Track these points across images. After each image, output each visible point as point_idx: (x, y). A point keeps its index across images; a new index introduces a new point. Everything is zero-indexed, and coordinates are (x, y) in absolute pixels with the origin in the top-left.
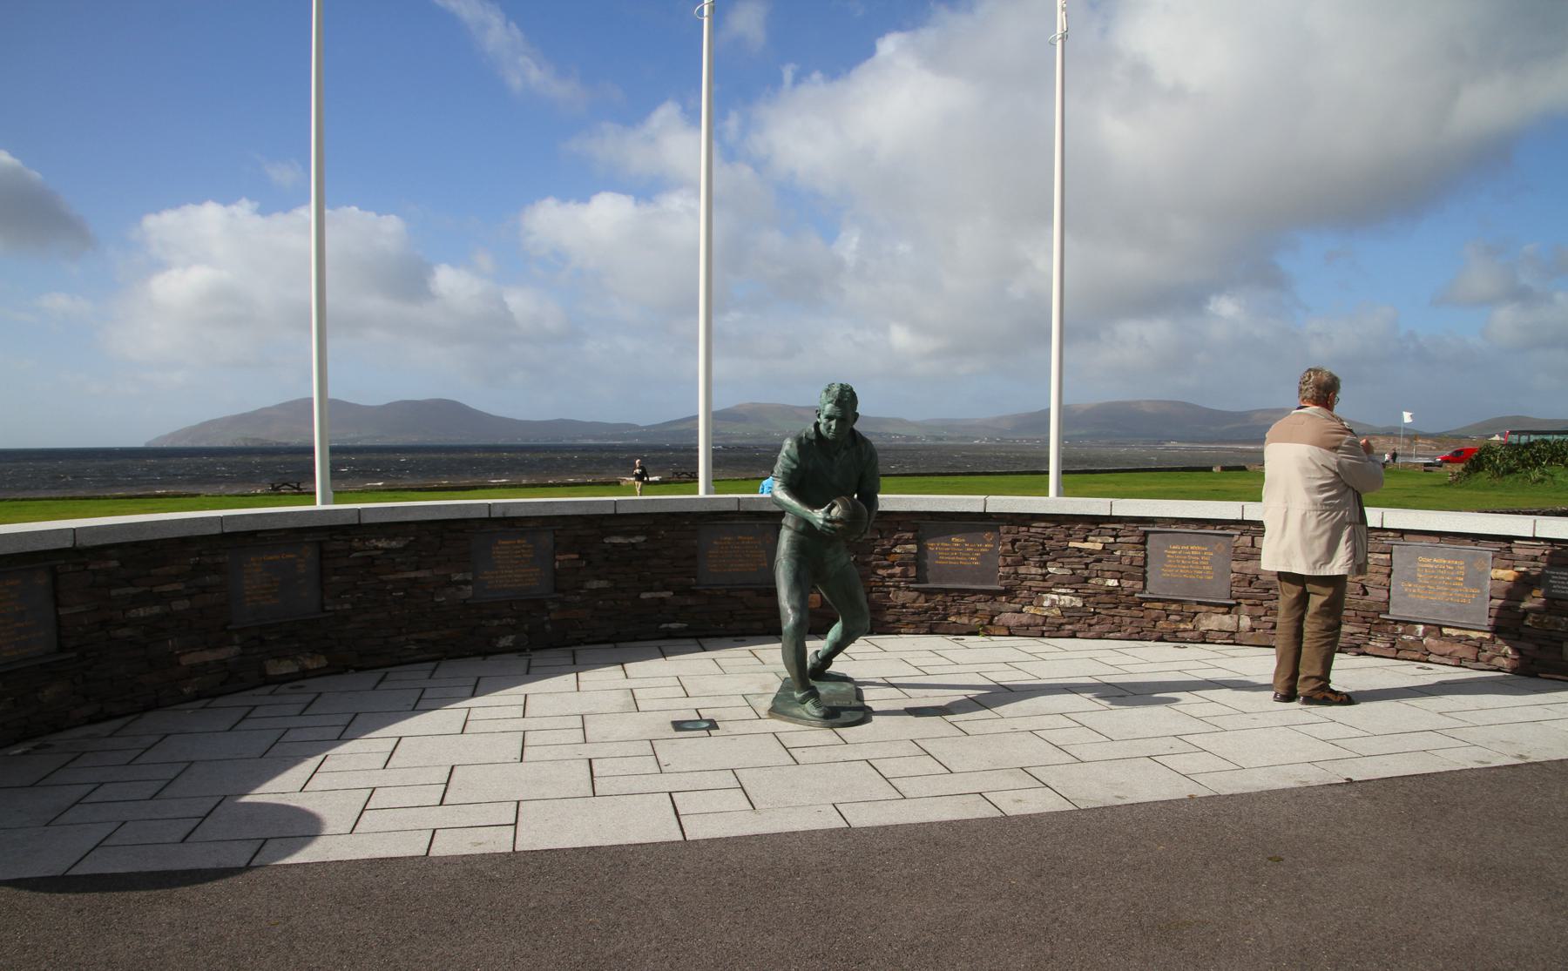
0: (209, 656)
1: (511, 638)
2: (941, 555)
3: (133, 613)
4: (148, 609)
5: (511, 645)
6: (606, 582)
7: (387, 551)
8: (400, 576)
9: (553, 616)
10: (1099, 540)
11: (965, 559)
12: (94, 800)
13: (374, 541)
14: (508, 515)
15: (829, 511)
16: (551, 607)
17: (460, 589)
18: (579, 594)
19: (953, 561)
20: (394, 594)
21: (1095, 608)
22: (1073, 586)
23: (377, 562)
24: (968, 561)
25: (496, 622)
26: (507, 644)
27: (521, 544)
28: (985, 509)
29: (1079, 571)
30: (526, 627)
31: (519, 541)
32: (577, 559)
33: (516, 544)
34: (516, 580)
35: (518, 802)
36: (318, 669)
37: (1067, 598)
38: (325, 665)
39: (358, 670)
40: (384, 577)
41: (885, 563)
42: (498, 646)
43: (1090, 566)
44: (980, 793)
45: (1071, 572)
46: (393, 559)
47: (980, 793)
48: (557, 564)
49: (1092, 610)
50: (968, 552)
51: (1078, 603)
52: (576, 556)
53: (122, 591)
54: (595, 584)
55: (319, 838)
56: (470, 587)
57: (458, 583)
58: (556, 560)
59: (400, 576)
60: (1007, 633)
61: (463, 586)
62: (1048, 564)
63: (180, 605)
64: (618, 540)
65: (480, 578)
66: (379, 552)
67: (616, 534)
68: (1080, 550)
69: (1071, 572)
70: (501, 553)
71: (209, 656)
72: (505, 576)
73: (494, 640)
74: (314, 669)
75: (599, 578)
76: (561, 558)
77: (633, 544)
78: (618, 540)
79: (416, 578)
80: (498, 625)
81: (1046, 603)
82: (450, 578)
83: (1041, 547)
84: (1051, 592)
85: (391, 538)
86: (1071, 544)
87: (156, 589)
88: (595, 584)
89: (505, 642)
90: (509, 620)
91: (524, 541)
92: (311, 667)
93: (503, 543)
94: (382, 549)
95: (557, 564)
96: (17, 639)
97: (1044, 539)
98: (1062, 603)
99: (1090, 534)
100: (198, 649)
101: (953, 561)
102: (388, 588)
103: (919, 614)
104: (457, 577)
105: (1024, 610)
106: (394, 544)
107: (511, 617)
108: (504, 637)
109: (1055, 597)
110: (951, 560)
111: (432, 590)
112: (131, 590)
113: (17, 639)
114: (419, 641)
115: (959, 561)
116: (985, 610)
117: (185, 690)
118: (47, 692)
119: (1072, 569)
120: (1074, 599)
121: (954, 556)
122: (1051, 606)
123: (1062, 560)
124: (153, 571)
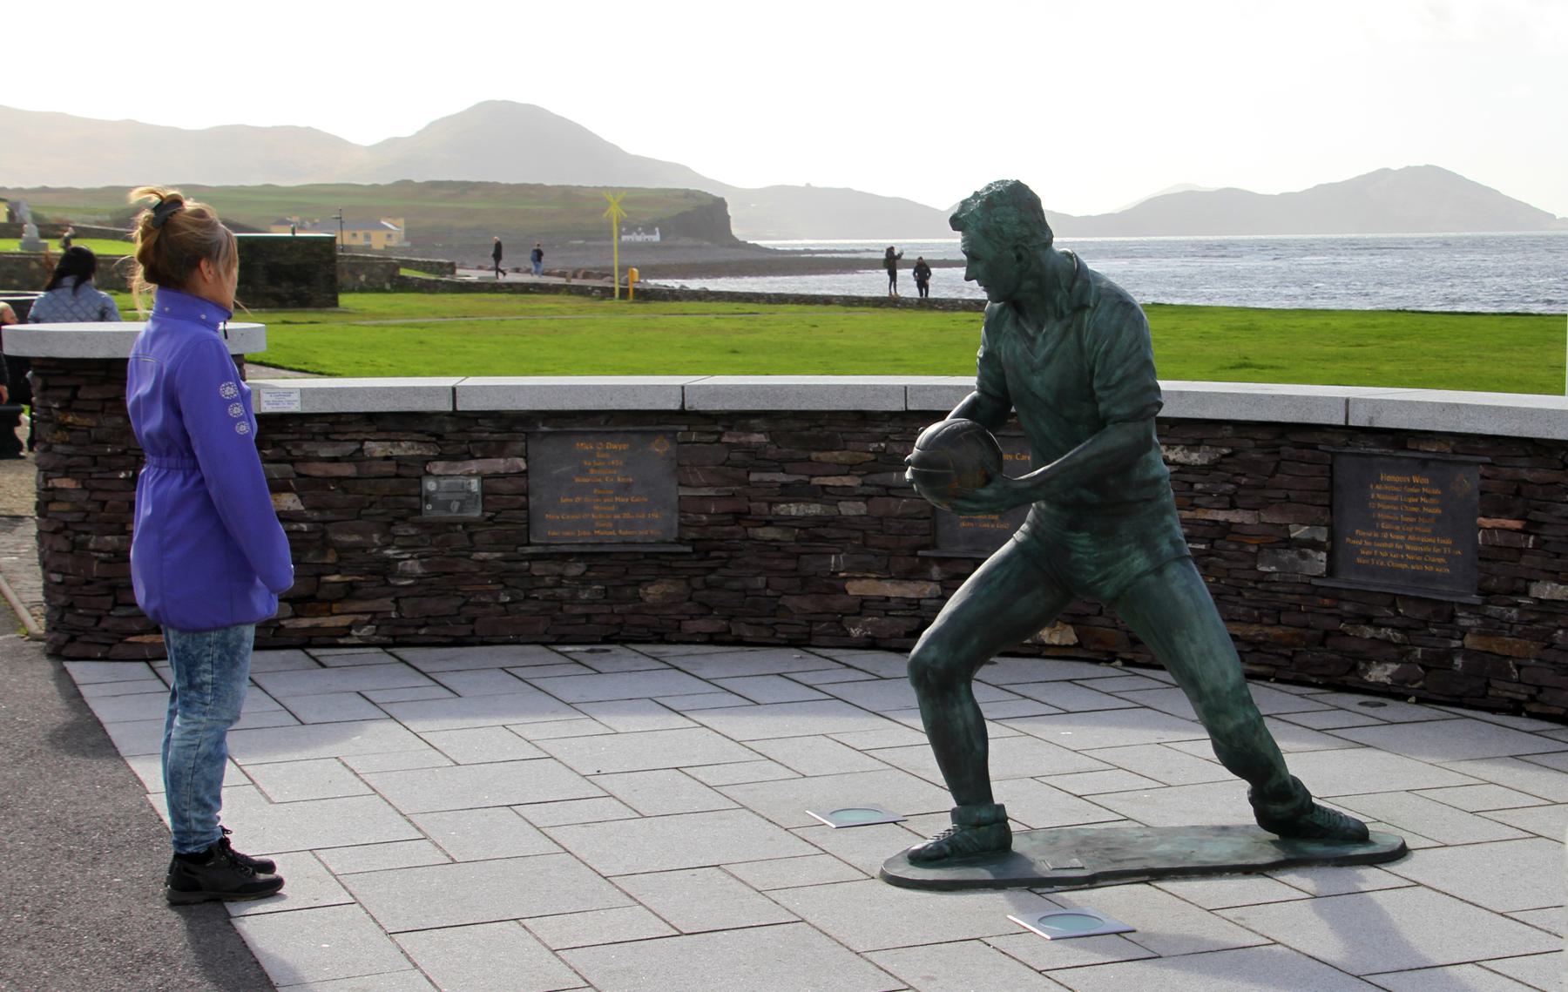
0: (891, 589)
1: (1392, 667)
3: (781, 509)
4: (802, 506)
5: (1389, 681)
9: (1469, 641)
12: (1296, 892)
14: (1376, 425)
16: (1466, 623)
17: (1304, 556)
18: (1518, 605)
25: (1369, 632)
26: (1383, 679)
27: (1419, 486)
30: (1419, 652)
31: (1416, 480)
32: (1518, 531)
33: (1411, 485)
36: (1059, 646)
38: (1071, 643)
39: (1128, 663)
42: (1366, 677)
53: (767, 477)
55: (393, 726)
63: (850, 509)
65: (1348, 539)
70: (1384, 497)
71: (891, 589)
72: (1391, 546)
74: (1053, 646)
76: (1488, 523)
80: (1373, 638)
82: (1288, 531)
85: (1193, 446)
87: (815, 481)
89: (1380, 673)
90: (1389, 631)
91: (1426, 481)
92: (1047, 641)
93: (1389, 478)
96: (618, 517)
100: (874, 576)
104: (1298, 532)
106: (1195, 458)
107: (1394, 628)
108: (1379, 663)
111: (1253, 549)
112: (781, 478)
113: (618, 517)
117: (852, 631)
118: (651, 590)
124: (814, 455)
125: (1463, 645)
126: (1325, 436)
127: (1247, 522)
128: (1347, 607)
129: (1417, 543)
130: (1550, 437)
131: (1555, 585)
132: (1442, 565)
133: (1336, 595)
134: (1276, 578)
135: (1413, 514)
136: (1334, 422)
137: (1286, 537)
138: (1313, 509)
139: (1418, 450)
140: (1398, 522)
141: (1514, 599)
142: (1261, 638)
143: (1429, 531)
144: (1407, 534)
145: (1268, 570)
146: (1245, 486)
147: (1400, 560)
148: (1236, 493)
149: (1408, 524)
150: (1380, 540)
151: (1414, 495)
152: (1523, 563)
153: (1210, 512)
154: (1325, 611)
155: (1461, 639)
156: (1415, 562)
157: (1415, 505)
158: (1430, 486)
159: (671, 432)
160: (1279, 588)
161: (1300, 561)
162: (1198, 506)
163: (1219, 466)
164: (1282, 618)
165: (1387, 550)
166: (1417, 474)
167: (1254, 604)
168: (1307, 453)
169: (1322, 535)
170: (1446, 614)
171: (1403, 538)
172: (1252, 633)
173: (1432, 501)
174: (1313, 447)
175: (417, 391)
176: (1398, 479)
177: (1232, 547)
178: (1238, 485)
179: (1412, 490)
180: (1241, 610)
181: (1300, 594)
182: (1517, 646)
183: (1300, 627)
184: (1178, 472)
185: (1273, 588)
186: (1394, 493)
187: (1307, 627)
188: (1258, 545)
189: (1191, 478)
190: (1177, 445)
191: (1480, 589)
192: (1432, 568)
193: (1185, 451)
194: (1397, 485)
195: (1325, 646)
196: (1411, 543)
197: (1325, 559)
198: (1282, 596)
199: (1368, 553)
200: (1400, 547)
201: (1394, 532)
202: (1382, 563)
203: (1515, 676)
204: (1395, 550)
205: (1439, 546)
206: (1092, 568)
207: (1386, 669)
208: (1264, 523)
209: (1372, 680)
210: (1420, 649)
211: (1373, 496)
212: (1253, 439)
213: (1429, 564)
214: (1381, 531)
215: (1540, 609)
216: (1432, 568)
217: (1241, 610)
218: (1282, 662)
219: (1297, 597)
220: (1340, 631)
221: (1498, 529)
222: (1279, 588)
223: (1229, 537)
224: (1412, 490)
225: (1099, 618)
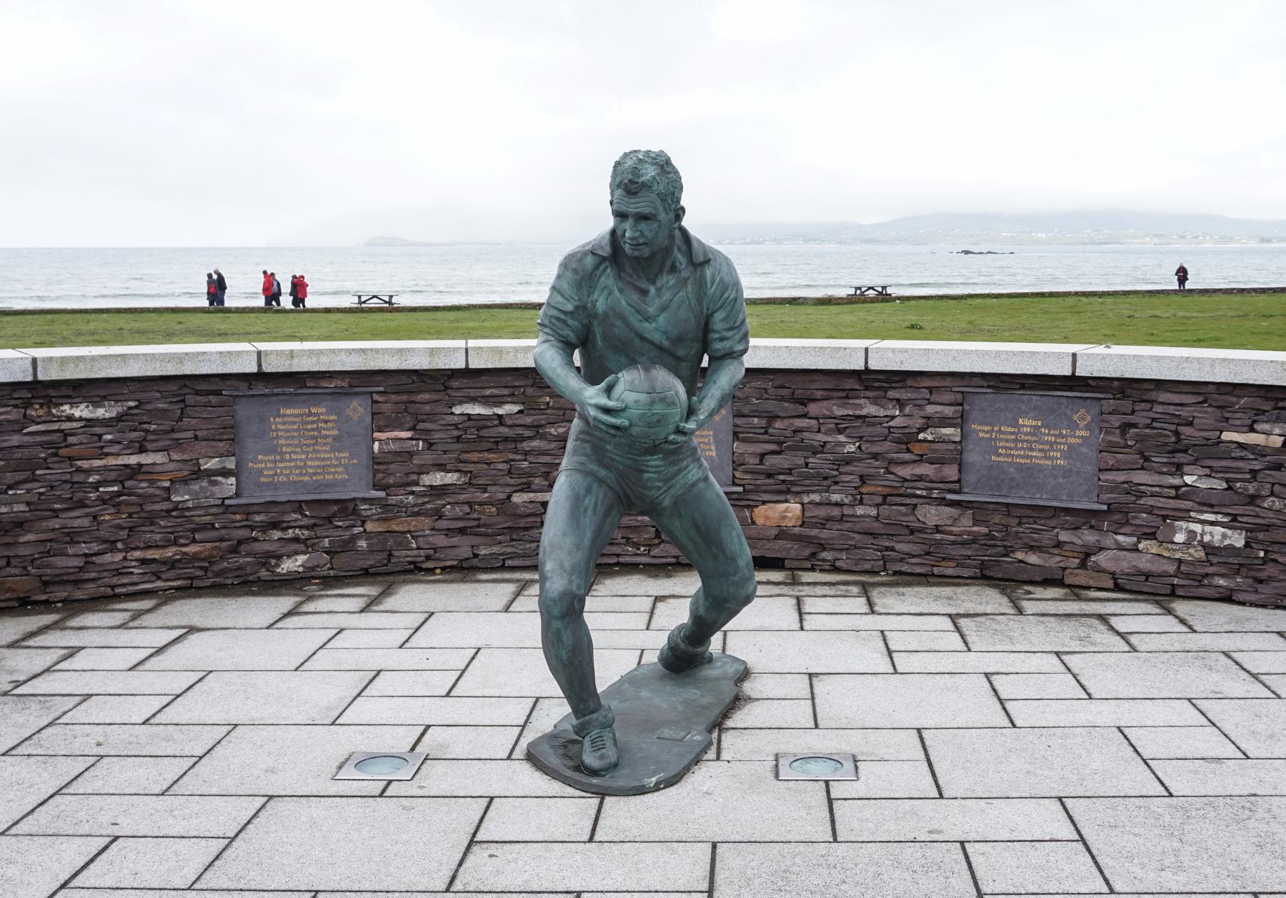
2: (1002, 448)
5: (301, 569)
6: (456, 475)
7: (90, 422)
8: (112, 461)
9: (370, 526)
10: (1277, 431)
11: (1040, 454)
13: (66, 407)
15: (383, 479)
18: (413, 493)
19: (1022, 457)
20: (101, 489)
21: (1266, 552)
22: (1229, 511)
23: (71, 440)
24: (1046, 458)
25: (276, 534)
28: (1074, 372)
29: (1238, 485)
32: (411, 439)
34: (310, 471)
35: (643, 651)
37: (1218, 530)
40: (85, 464)
41: (907, 456)
43: (1260, 476)
44: (1189, 700)
45: (1225, 485)
46: (100, 436)
47: (1189, 700)
48: (376, 445)
49: (1262, 554)
50: (1046, 443)
51: (1238, 540)
52: (408, 434)
54: (438, 478)
56: (232, 480)
57: (211, 473)
58: (374, 441)
59: (112, 461)
60: (1110, 584)
61: (219, 478)
62: (1186, 469)
64: (476, 409)
65: (250, 464)
66: (75, 425)
67: (473, 400)
68: (1241, 446)
69: (1225, 485)
73: (273, 562)
75: (442, 467)
77: (500, 417)
78: (476, 409)
79: (140, 465)
81: (1180, 538)
83: (1173, 439)
84: (1188, 519)
86: (1227, 436)
88: (438, 478)
90: (297, 531)
91: (324, 410)
93: (289, 412)
94: (81, 419)
95: (376, 445)
97: (1178, 425)
98: (1207, 538)
99: (1260, 417)
101: (1022, 457)
102: (91, 480)
103: (963, 544)
105: (1141, 546)
106: (101, 413)
107: (301, 527)
109: (1197, 528)
110: (1018, 456)
111: (167, 484)
114: (144, 562)
115: (1031, 457)
116: (1073, 543)
119: (1227, 481)
120: (1229, 532)
121: (1022, 448)
122: (1187, 544)
123: (1210, 463)
125: (365, 530)
126: (229, 383)
127: (158, 462)
128: (258, 518)
129: (317, 459)
130: (447, 367)
131: (443, 474)
132: (341, 473)
133: (247, 510)
134: (190, 504)
135: (313, 437)
136: (248, 370)
137: (196, 469)
138: (221, 444)
139: (317, 388)
140: (299, 446)
141: (409, 489)
142: (177, 557)
143: (328, 448)
144: (307, 453)
145: (182, 499)
146: (154, 432)
147: (301, 474)
148: (144, 440)
149: (308, 446)
150: (282, 461)
151: (313, 422)
152: (415, 462)
153: (121, 458)
154: (238, 524)
155: (362, 526)
156: (315, 474)
157: (313, 430)
158: (327, 414)
159: (368, 392)
160: (192, 513)
161: (210, 488)
162: (107, 455)
163: (125, 418)
164: (196, 537)
165: (290, 468)
166: (315, 406)
167: (170, 530)
168: (213, 399)
169: (230, 464)
170: (347, 508)
171: (303, 457)
172: (170, 554)
173: (330, 425)
174: (218, 393)
175: (180, 358)
176: (297, 411)
177: (144, 485)
178: (147, 431)
179: (311, 419)
180: (158, 537)
181: (213, 515)
182: (413, 523)
183: (214, 542)
184: (85, 426)
185: (187, 514)
186: (295, 423)
187: (221, 540)
188: (170, 480)
189: (98, 430)
190: (81, 403)
191: (374, 485)
192: (331, 477)
193: (91, 408)
194: (296, 416)
195: (238, 552)
196: (312, 459)
197: (234, 483)
198: (197, 519)
199: (271, 473)
200: (302, 464)
201: (296, 453)
202: (285, 479)
203: (414, 546)
204: (297, 467)
205: (337, 459)
206: (660, 484)
207: (296, 560)
208: (173, 461)
209: (285, 572)
210: (327, 540)
211: (273, 427)
212: (159, 391)
213: (329, 473)
214: (282, 453)
215: (433, 492)
216: (331, 477)
217: (158, 537)
218: (199, 573)
219: (209, 517)
220: (253, 538)
221: (392, 439)
222: (192, 513)
223: (140, 477)
224: (311, 419)
225: (8, 569)
